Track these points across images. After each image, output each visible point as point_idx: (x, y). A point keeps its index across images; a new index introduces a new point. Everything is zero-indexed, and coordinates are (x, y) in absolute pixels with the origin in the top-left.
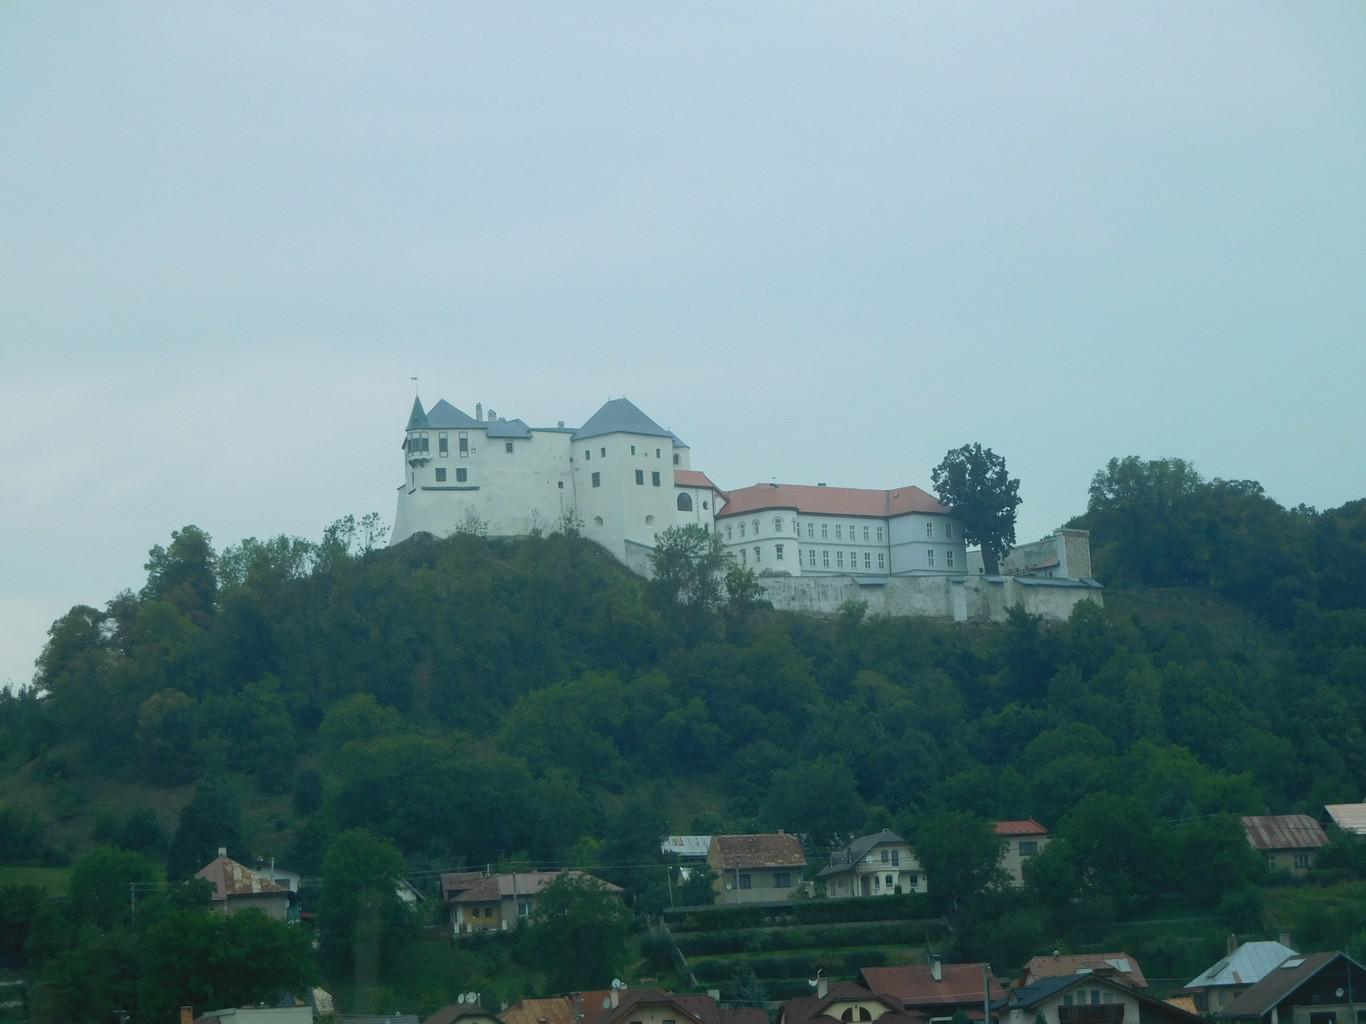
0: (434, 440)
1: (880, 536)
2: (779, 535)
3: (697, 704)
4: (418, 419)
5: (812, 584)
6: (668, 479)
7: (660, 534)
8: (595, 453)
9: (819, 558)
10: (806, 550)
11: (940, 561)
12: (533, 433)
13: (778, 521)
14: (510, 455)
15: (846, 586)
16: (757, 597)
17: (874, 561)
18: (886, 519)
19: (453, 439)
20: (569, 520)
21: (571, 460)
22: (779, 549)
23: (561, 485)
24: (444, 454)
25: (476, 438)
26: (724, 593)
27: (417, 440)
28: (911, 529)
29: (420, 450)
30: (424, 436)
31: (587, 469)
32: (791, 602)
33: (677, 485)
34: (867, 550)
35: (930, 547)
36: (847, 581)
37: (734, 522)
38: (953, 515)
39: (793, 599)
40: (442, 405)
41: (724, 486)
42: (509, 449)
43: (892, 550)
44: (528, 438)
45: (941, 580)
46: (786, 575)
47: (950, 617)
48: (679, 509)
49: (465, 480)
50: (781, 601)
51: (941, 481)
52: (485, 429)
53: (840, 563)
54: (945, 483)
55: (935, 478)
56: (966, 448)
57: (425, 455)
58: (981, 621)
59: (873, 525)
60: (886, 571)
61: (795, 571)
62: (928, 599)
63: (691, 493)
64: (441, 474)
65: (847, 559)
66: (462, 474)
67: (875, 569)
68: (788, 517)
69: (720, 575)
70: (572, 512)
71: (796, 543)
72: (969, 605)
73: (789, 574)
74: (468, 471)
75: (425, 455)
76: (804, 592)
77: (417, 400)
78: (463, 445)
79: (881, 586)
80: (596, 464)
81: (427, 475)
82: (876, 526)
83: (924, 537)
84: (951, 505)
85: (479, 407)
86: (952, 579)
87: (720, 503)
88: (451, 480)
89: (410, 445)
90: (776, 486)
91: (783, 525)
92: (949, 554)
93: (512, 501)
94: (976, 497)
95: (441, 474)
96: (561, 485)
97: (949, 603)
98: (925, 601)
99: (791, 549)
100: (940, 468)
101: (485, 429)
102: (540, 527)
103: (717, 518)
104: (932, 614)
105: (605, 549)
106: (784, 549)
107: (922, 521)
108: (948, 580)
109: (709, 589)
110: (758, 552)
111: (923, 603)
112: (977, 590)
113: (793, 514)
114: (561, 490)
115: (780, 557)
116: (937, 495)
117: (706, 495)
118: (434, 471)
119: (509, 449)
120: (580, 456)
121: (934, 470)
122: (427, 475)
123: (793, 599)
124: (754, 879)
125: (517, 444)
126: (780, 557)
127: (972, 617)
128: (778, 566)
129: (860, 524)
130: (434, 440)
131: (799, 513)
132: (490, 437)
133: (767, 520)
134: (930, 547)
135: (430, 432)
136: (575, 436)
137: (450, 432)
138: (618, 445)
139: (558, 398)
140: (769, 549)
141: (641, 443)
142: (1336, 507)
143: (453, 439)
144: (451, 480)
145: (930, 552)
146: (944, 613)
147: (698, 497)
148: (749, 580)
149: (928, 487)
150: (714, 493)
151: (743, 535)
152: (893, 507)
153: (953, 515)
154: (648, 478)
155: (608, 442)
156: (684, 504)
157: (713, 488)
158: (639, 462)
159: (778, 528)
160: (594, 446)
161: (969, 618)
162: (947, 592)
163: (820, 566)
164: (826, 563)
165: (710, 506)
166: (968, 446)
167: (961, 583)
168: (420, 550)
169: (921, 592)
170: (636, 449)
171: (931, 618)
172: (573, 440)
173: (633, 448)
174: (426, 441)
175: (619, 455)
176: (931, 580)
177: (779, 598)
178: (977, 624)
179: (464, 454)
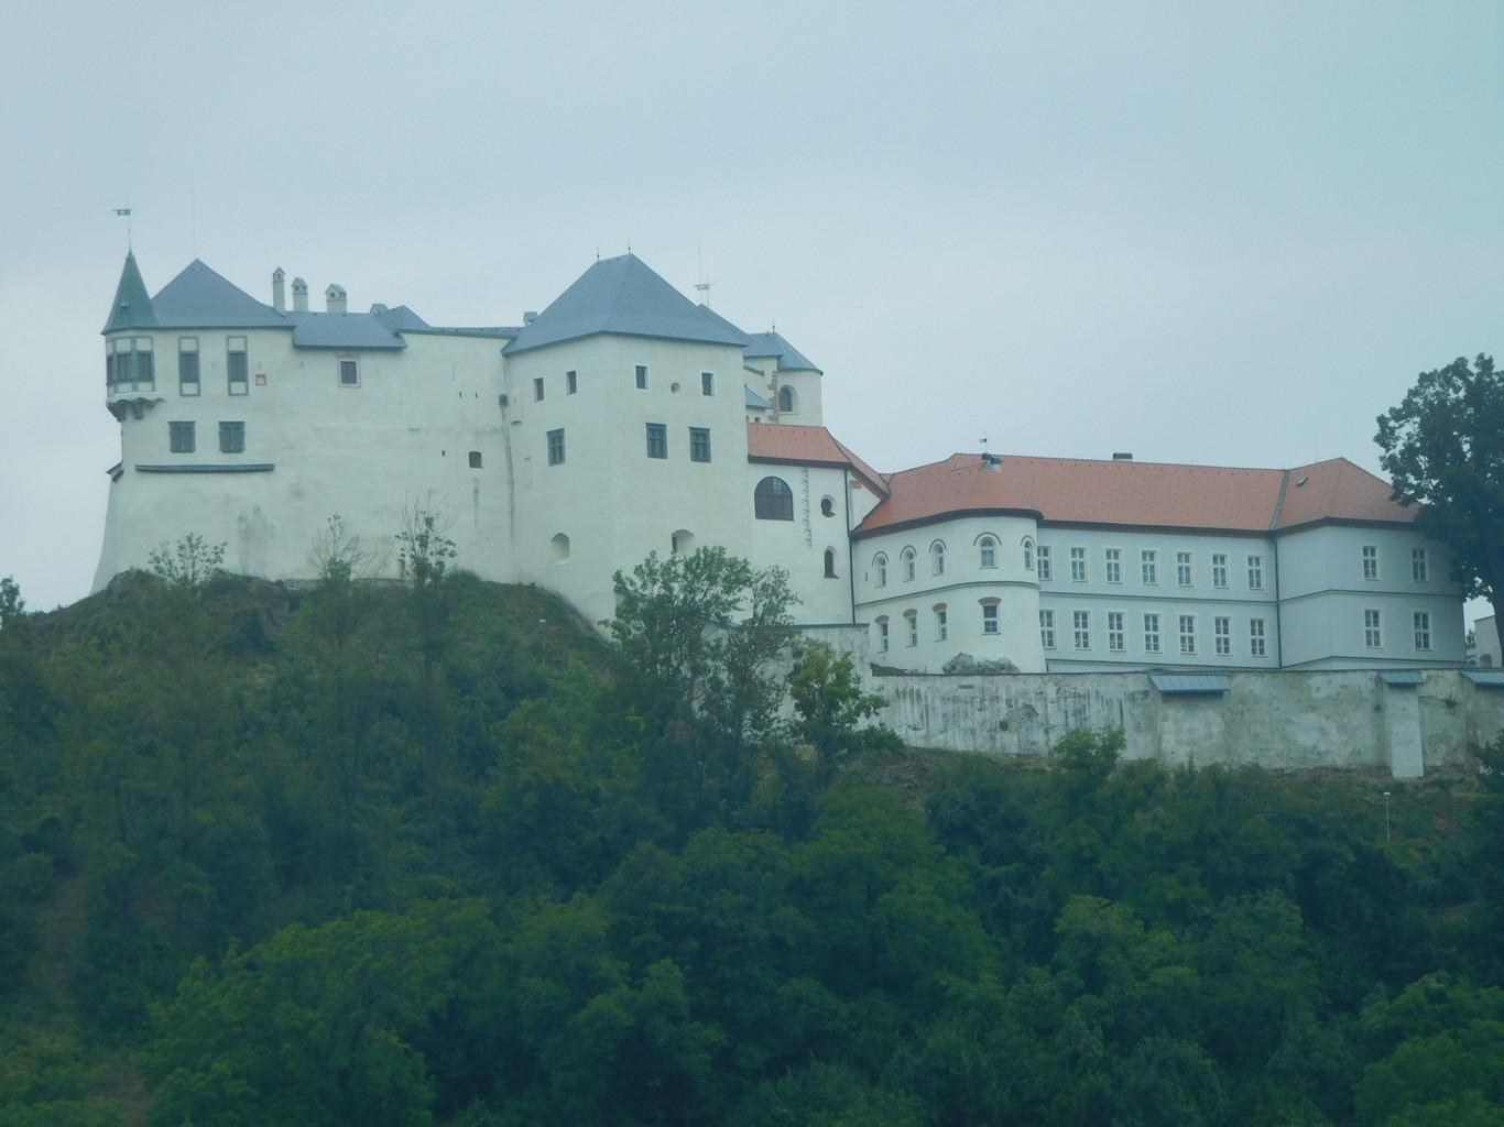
0: (166, 357)
1: (1255, 579)
2: (990, 575)
3: (667, 978)
4: (132, 307)
5: (1051, 691)
6: (730, 444)
7: (628, 573)
8: (556, 386)
9: (1099, 632)
10: (1064, 612)
11: (1396, 641)
12: (407, 338)
13: (987, 542)
14: (348, 390)
15: (1132, 697)
16: (862, 723)
17: (1240, 637)
18: (1271, 537)
19: (213, 352)
20: (423, 540)
21: (504, 401)
22: (990, 608)
23: (475, 460)
24: (190, 388)
25: (267, 351)
26: (787, 711)
27: (126, 355)
28: (1322, 560)
29: (131, 380)
30: (143, 345)
31: (538, 420)
32: (999, 735)
33: (753, 459)
34: (1151, 609)
36: (1135, 684)
37: (892, 545)
38: (1428, 526)
39: (1004, 726)
40: (197, 274)
41: (882, 462)
42: (349, 375)
43: (1284, 609)
44: (396, 350)
45: (1363, 683)
46: (1004, 670)
47: (1383, 769)
48: (758, 517)
49: (239, 449)
50: (973, 732)
51: (1400, 446)
52: (291, 328)
53: (1153, 643)
54: (1410, 451)
55: (1385, 437)
56: (1459, 368)
57: (144, 391)
58: (1456, 777)
59: (1238, 554)
60: (1269, 660)
61: (1030, 658)
62: (1331, 727)
63: (792, 477)
64: (182, 435)
65: (1169, 632)
66: (232, 435)
67: (1206, 654)
68: (1014, 535)
69: (774, 670)
70: (429, 522)
71: (1034, 594)
72: (1429, 742)
73: (1011, 667)
74: (247, 428)
75: (144, 391)
76: (1030, 712)
77: (130, 263)
78: (237, 366)
79: (1216, 695)
80: (558, 409)
81: (156, 429)
82: (1176, 551)
83: (1358, 580)
84: (1425, 501)
85: (278, 276)
86: (1389, 678)
87: (865, 501)
88: (207, 449)
89: (121, 368)
90: (993, 460)
91: (1000, 552)
92: (1421, 620)
93: (333, 495)
95: (182, 435)
96: (475, 460)
97: (1382, 745)
98: (1324, 732)
99: (1020, 609)
100: (1398, 415)
101: (291, 328)
102: (347, 558)
103: (856, 537)
104: (1340, 762)
105: (574, 611)
106: (1001, 608)
108: (1379, 680)
109: (751, 695)
110: (913, 621)
111: (1312, 737)
112: (1450, 704)
113: (1028, 527)
114: (476, 470)
115: (991, 628)
116: (1387, 477)
117: (831, 483)
118: (167, 428)
119: (349, 375)
120: (522, 391)
121: (1382, 420)
122: (156, 429)
123: (1004, 726)
125: (366, 365)
126: (991, 628)
127: (1436, 769)
128: (985, 650)
129: (1202, 551)
130: (166, 357)
131: (1043, 523)
132: (299, 348)
133: (962, 538)
135: (157, 336)
136: (513, 345)
138: (606, 363)
139: (487, 269)
140: (966, 609)
141: (663, 362)
143: (213, 352)
144: (207, 449)
145: (1373, 617)
146: (1369, 758)
147: (807, 488)
148: (842, 679)
149: (1370, 459)
150: (851, 478)
151: (912, 576)
152: (1285, 510)
153: (1428, 526)
154: (678, 442)
155: (585, 358)
156: (773, 502)
157: (847, 466)
158: (654, 404)
159: (988, 559)
160: (552, 367)
161: (1429, 770)
162: (1378, 708)
163: (1100, 648)
164: (1117, 641)
165: (838, 508)
166: (1462, 362)
167: (1410, 687)
169: (1314, 709)
170: (649, 375)
171: (1336, 770)
172: (508, 355)
173: (641, 371)
174: (146, 358)
175: (606, 387)
176: (1339, 679)
177: (969, 723)
178: (1443, 785)
179: (238, 387)
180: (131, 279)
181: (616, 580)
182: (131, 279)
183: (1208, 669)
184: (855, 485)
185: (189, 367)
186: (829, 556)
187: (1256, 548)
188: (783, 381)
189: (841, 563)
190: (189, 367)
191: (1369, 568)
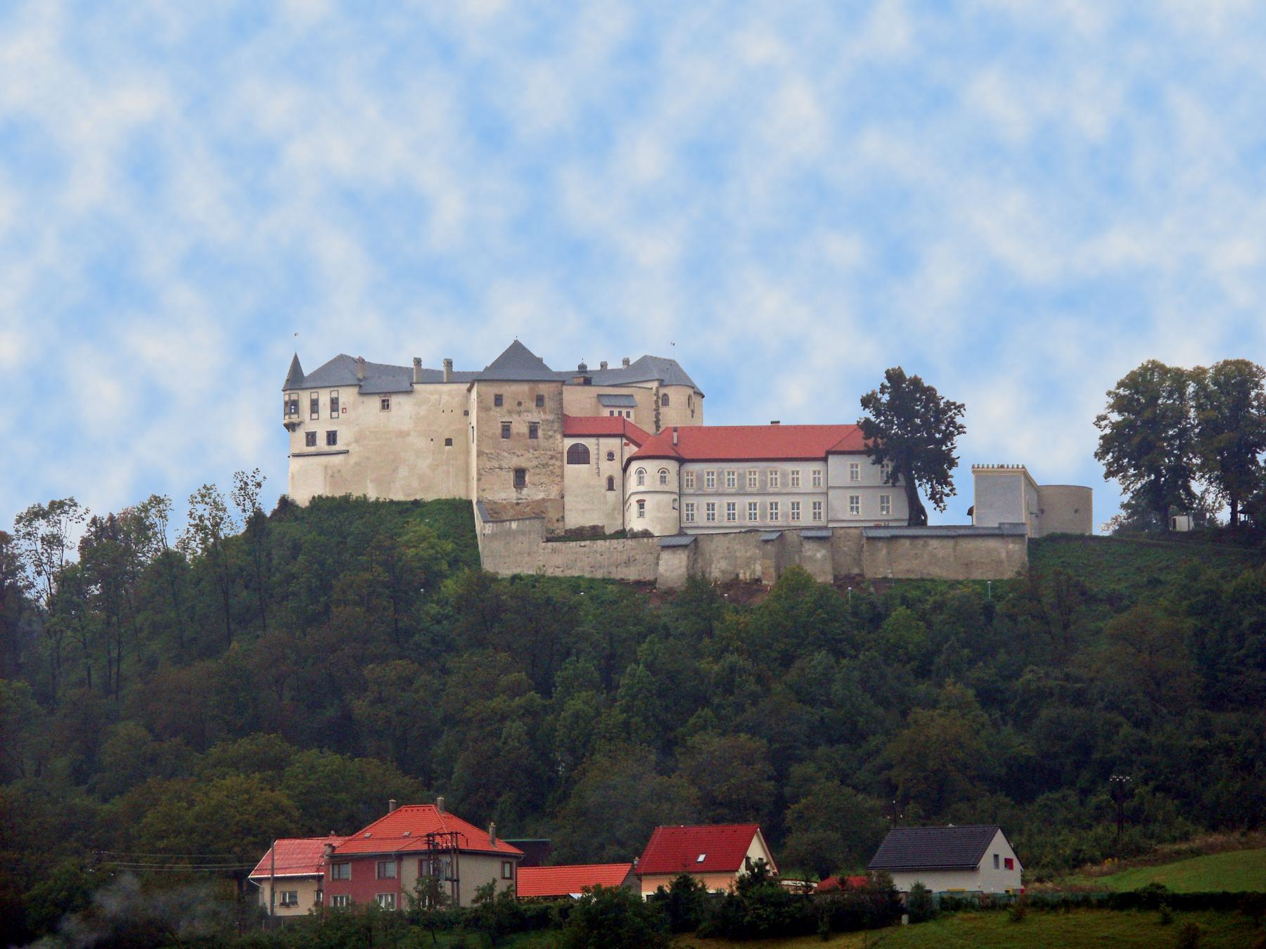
1: (816, 482)
14: (385, 414)
18: (682, 461)
28: (839, 468)
34: (796, 499)
35: (854, 493)
42: (385, 405)
63: (589, 443)
64: (311, 438)
66: (332, 438)
78: (334, 403)
81: (300, 434)
94: (908, 431)
95: (311, 438)
107: (848, 460)
122: (300, 434)
124: (1029, 915)
125: (394, 400)
130: (305, 399)
134: (854, 493)
137: (341, 390)
142: (784, 423)
150: (624, 441)
165: (617, 456)
168: (281, 528)
179: (335, 414)
180: (296, 363)
181: (52, 504)
182: (296, 363)
183: (944, 532)
184: (626, 445)
185: (314, 405)
186: (611, 480)
187: (817, 466)
188: (662, 391)
189: (617, 483)
190: (314, 405)
191: (853, 475)
